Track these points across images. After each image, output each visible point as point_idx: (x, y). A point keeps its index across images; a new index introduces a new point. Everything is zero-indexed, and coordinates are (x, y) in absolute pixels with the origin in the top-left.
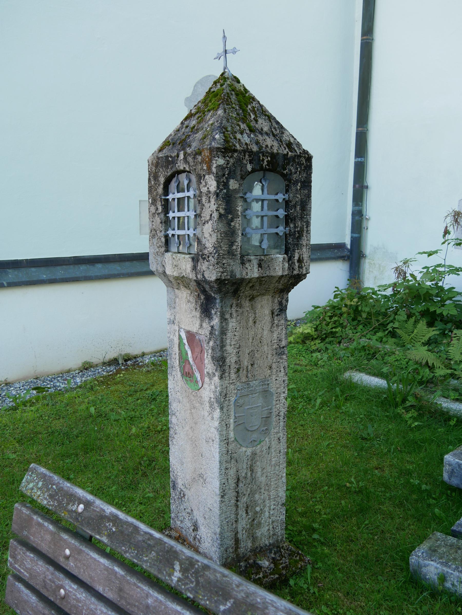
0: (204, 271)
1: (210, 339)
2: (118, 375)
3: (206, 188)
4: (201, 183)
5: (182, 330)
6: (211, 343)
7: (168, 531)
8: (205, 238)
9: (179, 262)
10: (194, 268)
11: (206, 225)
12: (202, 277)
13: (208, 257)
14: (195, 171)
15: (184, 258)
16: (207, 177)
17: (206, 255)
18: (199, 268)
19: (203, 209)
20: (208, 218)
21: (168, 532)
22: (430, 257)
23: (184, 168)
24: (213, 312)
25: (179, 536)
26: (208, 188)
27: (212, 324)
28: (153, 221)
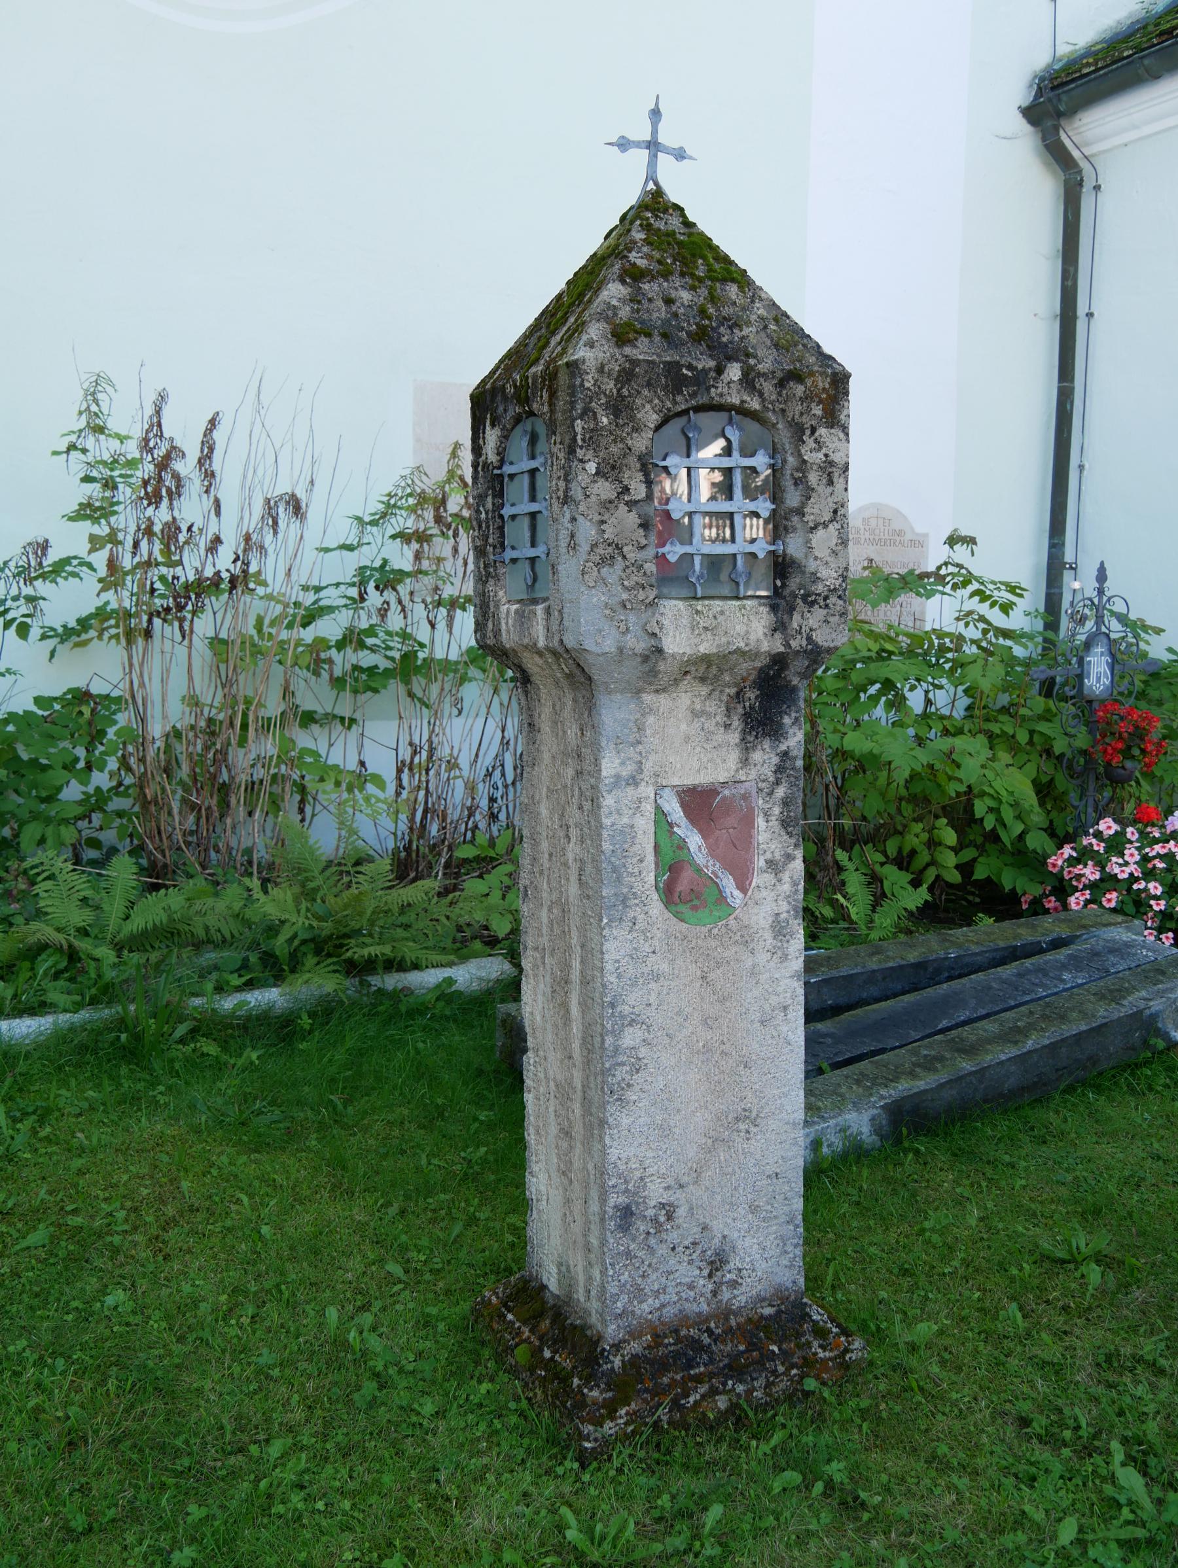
0: (811, 630)
1: (777, 783)
2: (950, 837)
3: (821, 455)
4: (804, 442)
5: (667, 792)
6: (780, 792)
7: (615, 1356)
8: (816, 558)
9: (720, 618)
10: (780, 627)
11: (821, 532)
12: (804, 643)
13: (826, 598)
14: (784, 416)
15: (744, 607)
16: (822, 431)
17: (819, 595)
18: (795, 625)
19: (809, 498)
20: (827, 516)
21: (619, 1357)
22: (85, 484)
23: (743, 402)
24: (787, 720)
25: (656, 1336)
26: (826, 455)
27: (783, 747)
28: (603, 522)
